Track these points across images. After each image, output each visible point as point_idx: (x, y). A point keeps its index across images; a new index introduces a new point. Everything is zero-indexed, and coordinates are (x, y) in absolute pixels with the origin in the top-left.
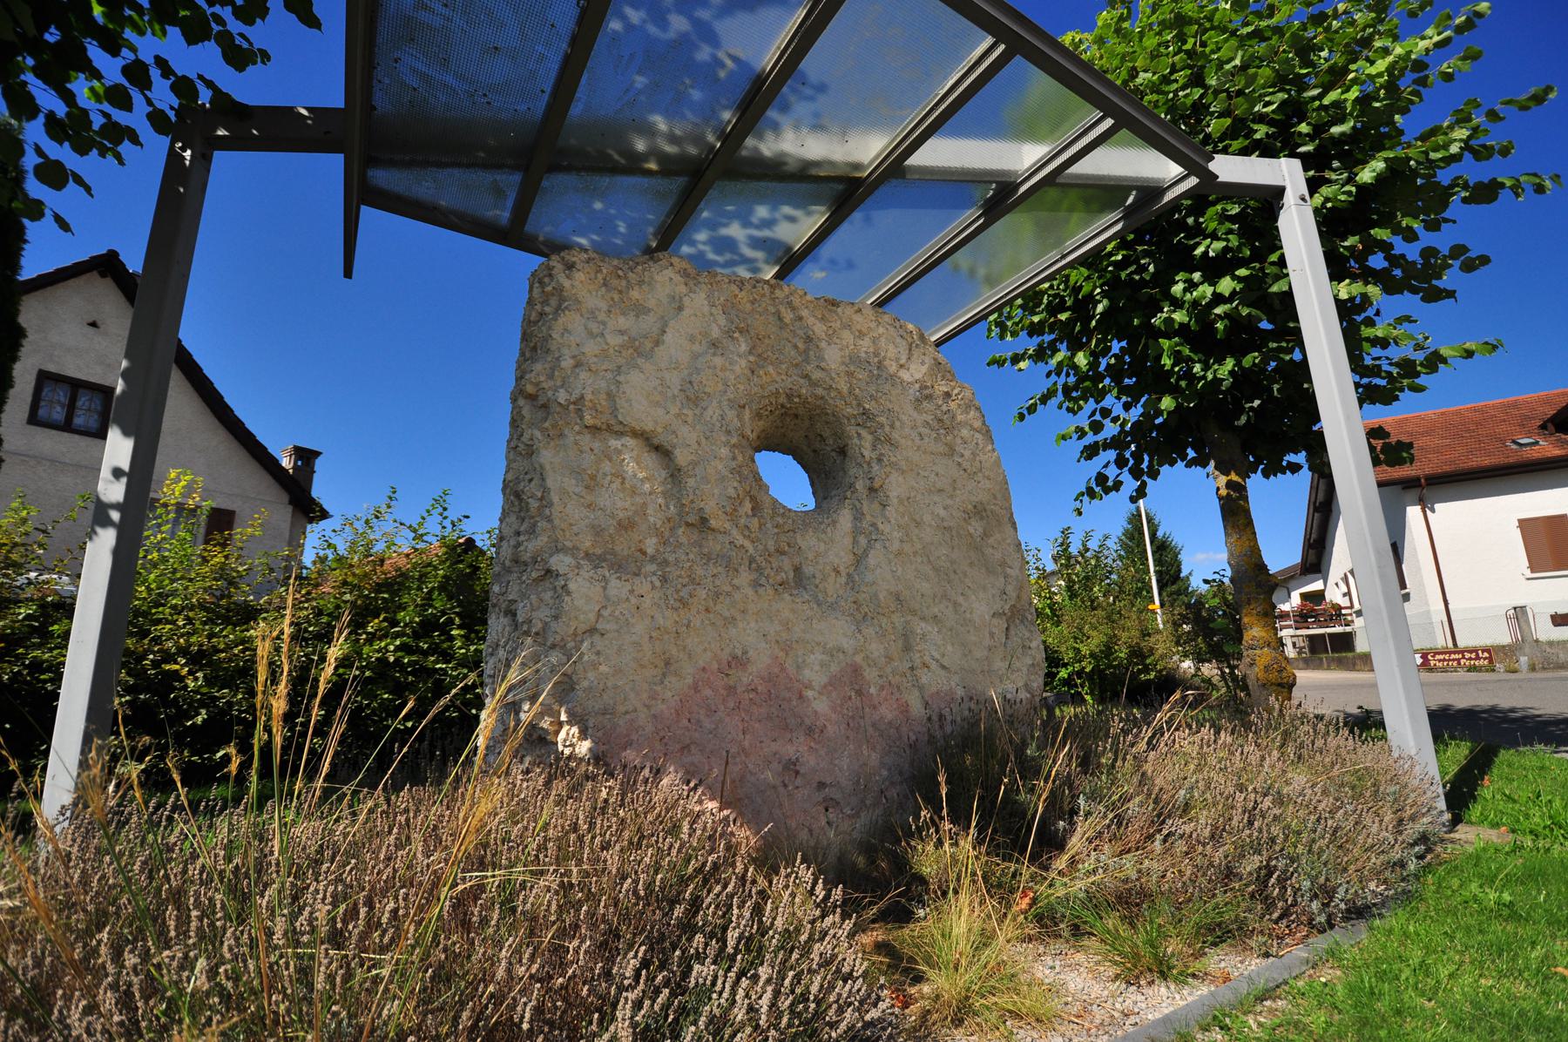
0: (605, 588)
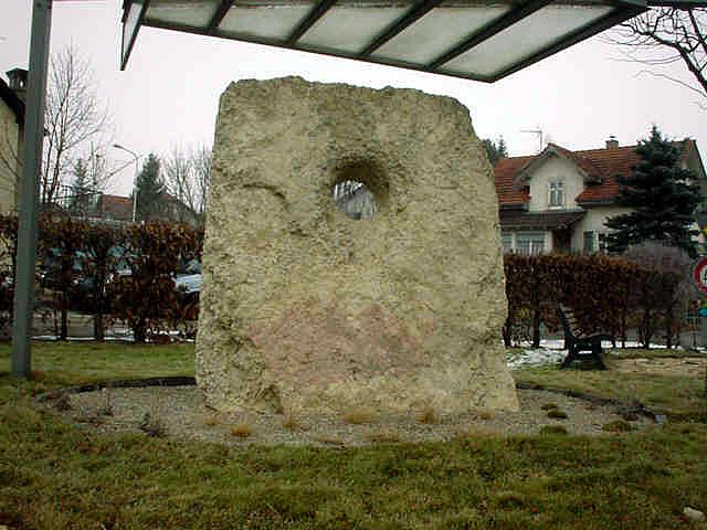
0: (655, 472)
